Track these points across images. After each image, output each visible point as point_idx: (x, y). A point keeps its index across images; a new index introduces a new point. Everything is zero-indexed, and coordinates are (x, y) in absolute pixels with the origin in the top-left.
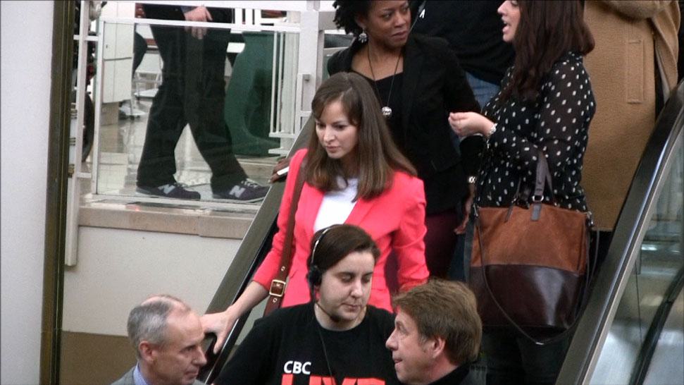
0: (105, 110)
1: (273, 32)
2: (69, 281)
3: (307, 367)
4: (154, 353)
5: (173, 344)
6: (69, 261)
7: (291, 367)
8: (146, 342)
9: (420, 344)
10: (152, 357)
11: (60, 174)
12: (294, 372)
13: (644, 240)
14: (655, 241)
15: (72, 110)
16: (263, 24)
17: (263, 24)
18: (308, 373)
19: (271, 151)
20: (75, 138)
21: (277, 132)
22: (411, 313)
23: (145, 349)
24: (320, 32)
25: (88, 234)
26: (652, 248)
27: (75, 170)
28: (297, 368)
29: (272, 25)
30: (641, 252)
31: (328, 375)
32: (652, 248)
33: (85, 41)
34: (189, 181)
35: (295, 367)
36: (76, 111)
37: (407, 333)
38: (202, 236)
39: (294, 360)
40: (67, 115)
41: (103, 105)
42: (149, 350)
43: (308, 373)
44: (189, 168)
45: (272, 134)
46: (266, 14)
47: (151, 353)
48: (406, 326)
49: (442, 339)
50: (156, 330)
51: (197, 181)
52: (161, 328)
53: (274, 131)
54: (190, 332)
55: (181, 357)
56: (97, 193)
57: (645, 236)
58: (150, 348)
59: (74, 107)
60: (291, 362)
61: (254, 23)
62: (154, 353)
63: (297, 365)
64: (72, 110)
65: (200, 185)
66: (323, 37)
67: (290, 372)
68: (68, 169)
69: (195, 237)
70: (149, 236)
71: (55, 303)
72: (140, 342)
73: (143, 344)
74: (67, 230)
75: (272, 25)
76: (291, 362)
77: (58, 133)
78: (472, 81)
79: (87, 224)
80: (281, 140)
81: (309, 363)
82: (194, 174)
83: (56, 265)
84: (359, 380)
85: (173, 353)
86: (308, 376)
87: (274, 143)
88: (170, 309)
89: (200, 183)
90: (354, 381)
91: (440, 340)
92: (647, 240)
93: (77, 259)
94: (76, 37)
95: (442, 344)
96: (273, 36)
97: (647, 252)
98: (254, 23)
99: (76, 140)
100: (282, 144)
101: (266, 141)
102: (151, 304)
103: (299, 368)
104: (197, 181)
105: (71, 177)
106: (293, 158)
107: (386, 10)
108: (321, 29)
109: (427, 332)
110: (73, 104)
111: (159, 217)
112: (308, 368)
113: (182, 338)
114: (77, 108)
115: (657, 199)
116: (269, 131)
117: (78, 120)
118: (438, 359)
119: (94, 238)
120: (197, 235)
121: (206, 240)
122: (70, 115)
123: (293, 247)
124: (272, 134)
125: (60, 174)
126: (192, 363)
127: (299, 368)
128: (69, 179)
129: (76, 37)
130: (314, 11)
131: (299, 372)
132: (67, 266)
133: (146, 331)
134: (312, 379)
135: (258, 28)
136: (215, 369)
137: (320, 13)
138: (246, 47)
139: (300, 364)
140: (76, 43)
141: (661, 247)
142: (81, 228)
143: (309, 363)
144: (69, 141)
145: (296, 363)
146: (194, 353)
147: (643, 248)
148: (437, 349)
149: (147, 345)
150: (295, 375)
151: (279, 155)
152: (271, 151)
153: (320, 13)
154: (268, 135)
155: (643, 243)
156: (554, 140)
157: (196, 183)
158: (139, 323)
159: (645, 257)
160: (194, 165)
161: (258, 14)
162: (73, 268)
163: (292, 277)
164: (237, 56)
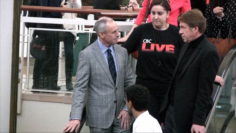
0: (31, 60)
1: (89, 33)
2: (18, 118)
4: (104, 35)
5: (109, 31)
6: (18, 112)
7: (145, 41)
8: (101, 32)
9: (191, 30)
10: (103, 36)
11: (15, 82)
12: (146, 42)
13: (217, 104)
14: (221, 104)
15: (19, 60)
16: (85, 30)
17: (85, 30)
18: (151, 42)
20: (20, 70)
22: (185, 22)
23: (101, 34)
25: (25, 102)
26: (220, 107)
27: (20, 80)
28: (147, 41)
29: (88, 30)
30: (216, 108)
31: (157, 43)
32: (220, 107)
34: (60, 84)
35: (147, 41)
36: (21, 60)
37: (185, 28)
38: (65, 103)
42: (102, 34)
43: (151, 42)
44: (60, 80)
46: (86, 27)
47: (103, 35)
48: (185, 26)
49: (197, 27)
50: (103, 28)
51: (63, 84)
52: (105, 27)
54: (114, 27)
55: (112, 35)
56: (28, 89)
57: (218, 103)
58: (102, 34)
60: (145, 39)
61: (82, 30)
62: (104, 35)
63: (147, 42)
64: (19, 60)
65: (63, 86)
67: (145, 42)
68: (18, 80)
69: (62, 104)
70: (46, 103)
71: (14, 126)
72: (99, 32)
73: (100, 33)
74: (18, 102)
75: (88, 30)
76: (145, 39)
77: (14, 68)
79: (25, 99)
81: (151, 40)
82: (61, 82)
83: (14, 113)
84: (167, 45)
85: (109, 34)
86: (151, 44)
88: (107, 21)
89: (63, 85)
90: (165, 45)
91: (197, 27)
92: (218, 104)
93: (21, 111)
95: (197, 28)
96: (89, 34)
97: (218, 108)
98: (82, 30)
99: (21, 70)
102: (101, 20)
103: (148, 41)
104: (63, 84)
105: (19, 83)
106: (130, 7)
109: (192, 26)
111: (50, 97)
112: (150, 41)
113: (112, 29)
115: (211, 117)
118: (197, 33)
119: (27, 104)
120: (63, 103)
121: (65, 104)
122: (19, 62)
125: (15, 82)
126: (115, 36)
127: (148, 41)
128: (18, 84)
131: (148, 42)
132: (18, 114)
133: (101, 28)
134: (152, 44)
135: (83, 32)
138: (79, 38)
139: (148, 40)
141: (223, 107)
142: (23, 101)
143: (151, 40)
144: (18, 71)
145: (147, 40)
146: (116, 33)
147: (217, 107)
148: (196, 30)
149: (101, 33)
150: (146, 43)
155: (217, 105)
156: (207, 31)
157: (62, 85)
158: (98, 26)
159: (218, 110)
160: (61, 79)
161: (83, 27)
162: (20, 114)
163: (126, 52)
164: (77, 41)
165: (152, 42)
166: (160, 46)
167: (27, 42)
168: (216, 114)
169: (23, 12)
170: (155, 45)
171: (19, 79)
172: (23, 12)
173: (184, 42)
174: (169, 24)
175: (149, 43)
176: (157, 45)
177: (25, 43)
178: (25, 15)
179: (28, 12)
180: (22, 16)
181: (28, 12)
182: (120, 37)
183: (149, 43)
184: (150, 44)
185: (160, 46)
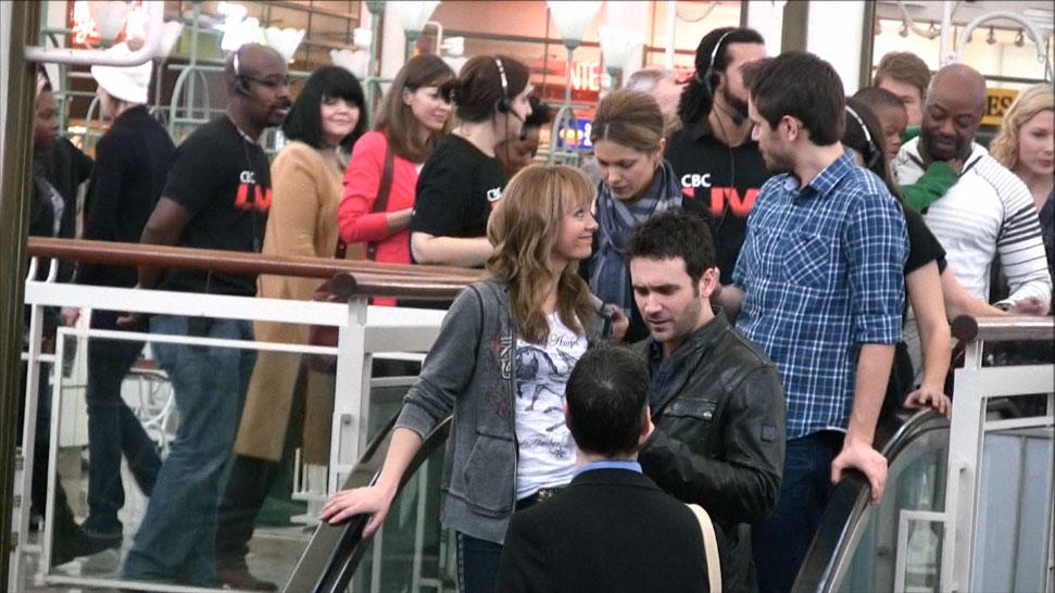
0: (62, 456)
3: (707, 180)
7: (689, 181)
15: (17, 456)
18: (708, 185)
19: (294, 519)
21: (303, 492)
24: (367, 355)
33: (37, 362)
36: (22, 460)
39: (692, 173)
40: (10, 464)
41: (60, 450)
43: (708, 185)
45: (296, 495)
53: (300, 490)
59: (20, 452)
60: (688, 176)
66: (370, 363)
67: (689, 185)
78: (637, 454)
80: (309, 505)
86: (709, 189)
87: (298, 508)
94: (24, 356)
100: (309, 508)
101: (286, 505)
105: (14, 550)
107: (519, 272)
108: (367, 351)
110: (18, 448)
112: (707, 180)
114: (24, 454)
116: (292, 491)
117: (24, 470)
123: (454, 449)
124: (296, 495)
128: (12, 554)
129: (24, 356)
130: (359, 326)
136: (354, 556)
137: (367, 329)
140: (25, 363)
150: (695, 188)
151: (304, 524)
152: (294, 519)
153: (367, 329)
154: (290, 497)
165: (714, 182)
166: (742, 196)
167: (988, 30)
168: (1019, 436)
169: (34, 261)
170: (724, 195)
171: (13, 536)
172: (34, 261)
173: (779, 58)
174: (30, 238)
175: (701, 186)
176: (733, 194)
177: (988, 30)
178: (42, 276)
179: (54, 263)
180: (51, 282)
181: (54, 263)
182: (152, 407)
183: (701, 186)
184: (709, 190)
185: (742, 196)
